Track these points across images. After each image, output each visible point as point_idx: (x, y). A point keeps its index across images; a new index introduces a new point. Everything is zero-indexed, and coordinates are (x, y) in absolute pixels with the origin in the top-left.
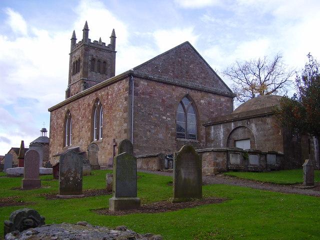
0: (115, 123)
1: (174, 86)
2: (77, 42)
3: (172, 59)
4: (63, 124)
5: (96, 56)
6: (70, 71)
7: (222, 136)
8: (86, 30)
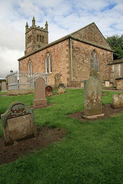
0: (60, 64)
2: (29, 27)
3: (87, 31)
4: (26, 67)
6: (26, 42)
7: (119, 70)
8: (34, 21)
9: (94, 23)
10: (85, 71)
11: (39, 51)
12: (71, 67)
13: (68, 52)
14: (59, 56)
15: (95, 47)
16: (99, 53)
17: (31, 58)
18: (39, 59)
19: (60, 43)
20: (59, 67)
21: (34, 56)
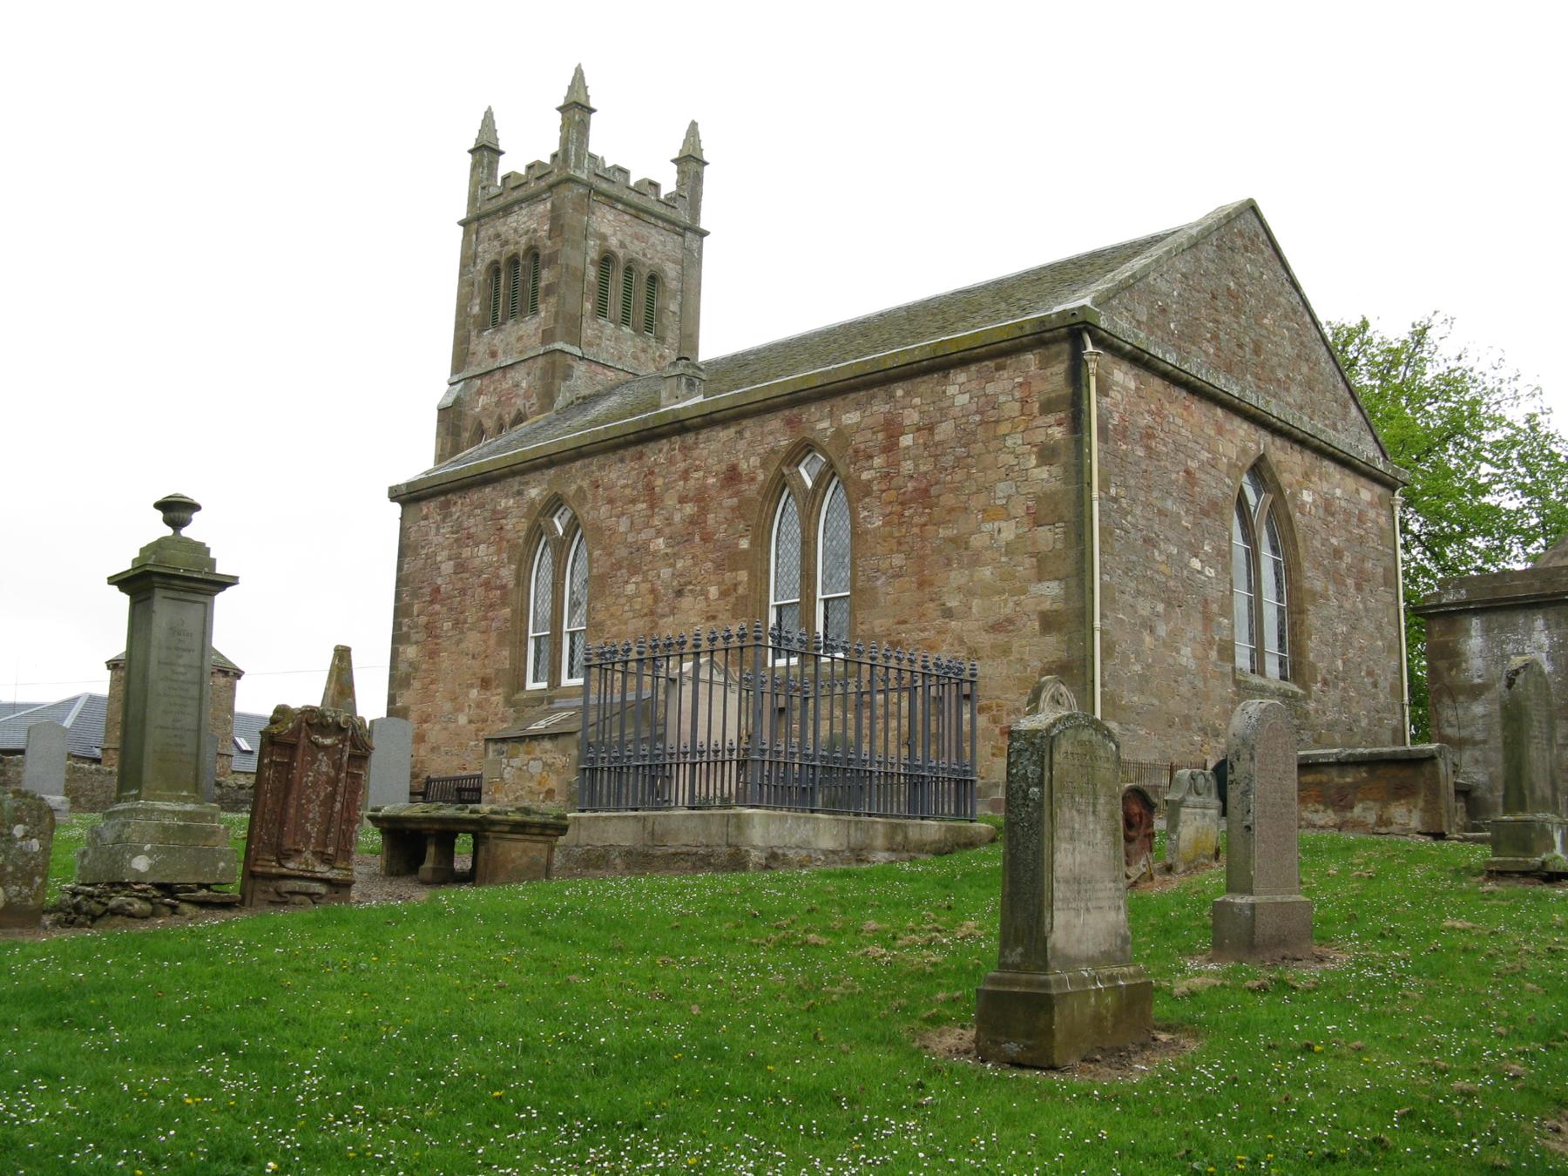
0: (957, 577)
1: (1219, 411)
2: (505, 167)
4: (507, 574)
5: (622, 245)
8: (576, 111)
9: (1252, 208)
10: (1192, 665)
11: (697, 429)
12: (1084, 616)
13: (1056, 470)
14: (948, 500)
15: (1263, 433)
16: (1294, 496)
17: (585, 484)
18: (689, 509)
19: (961, 377)
20: (948, 613)
21: (619, 474)
